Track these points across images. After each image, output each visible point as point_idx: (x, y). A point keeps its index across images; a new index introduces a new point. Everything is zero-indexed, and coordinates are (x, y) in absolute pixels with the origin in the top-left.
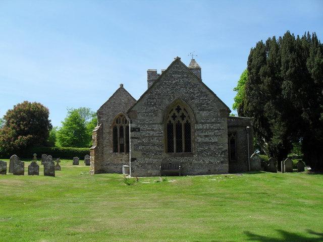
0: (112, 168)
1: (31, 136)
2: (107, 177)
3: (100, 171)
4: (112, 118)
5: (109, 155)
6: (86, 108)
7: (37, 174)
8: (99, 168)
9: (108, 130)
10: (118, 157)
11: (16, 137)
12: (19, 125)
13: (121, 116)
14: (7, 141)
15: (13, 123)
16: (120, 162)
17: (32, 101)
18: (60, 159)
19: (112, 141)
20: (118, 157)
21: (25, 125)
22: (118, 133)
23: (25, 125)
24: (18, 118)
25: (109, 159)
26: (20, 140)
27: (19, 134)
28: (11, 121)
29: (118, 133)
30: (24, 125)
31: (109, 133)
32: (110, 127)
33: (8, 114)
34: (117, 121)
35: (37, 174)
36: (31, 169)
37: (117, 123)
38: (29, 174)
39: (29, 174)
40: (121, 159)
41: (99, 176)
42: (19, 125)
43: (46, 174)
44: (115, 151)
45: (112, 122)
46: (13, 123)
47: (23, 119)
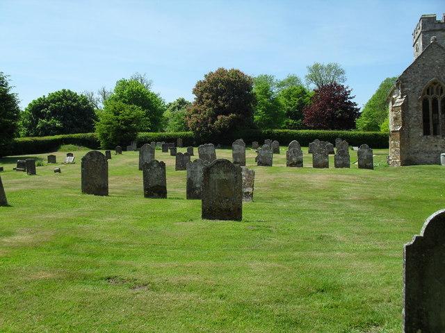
0: (423, 157)
1: (234, 115)
2: (24, 158)
3: (407, 161)
4: (421, 88)
5: (420, 141)
6: (269, 74)
7: (348, 166)
8: (405, 157)
9: (416, 104)
10: (432, 142)
11: (214, 118)
12: (216, 101)
13: (435, 83)
14: (202, 123)
15: (207, 98)
16: (435, 149)
17: (228, 67)
18: (216, 146)
19: (421, 119)
20: (432, 142)
21: (225, 101)
22: (431, 109)
23: (225, 101)
24: (213, 91)
25: (418, 145)
26: (221, 120)
27: (218, 114)
28: (204, 96)
29: (431, 109)
30: (223, 101)
31: (417, 108)
32: (419, 100)
33: (197, 86)
34: (428, 90)
35: (348, 166)
36: (338, 159)
37: (428, 94)
38: (337, 166)
39: (337, 166)
40: (436, 144)
41: (434, 169)
42: (216, 101)
43: (361, 167)
44: (426, 132)
45: (422, 93)
46: (207, 98)
47: (220, 93)
